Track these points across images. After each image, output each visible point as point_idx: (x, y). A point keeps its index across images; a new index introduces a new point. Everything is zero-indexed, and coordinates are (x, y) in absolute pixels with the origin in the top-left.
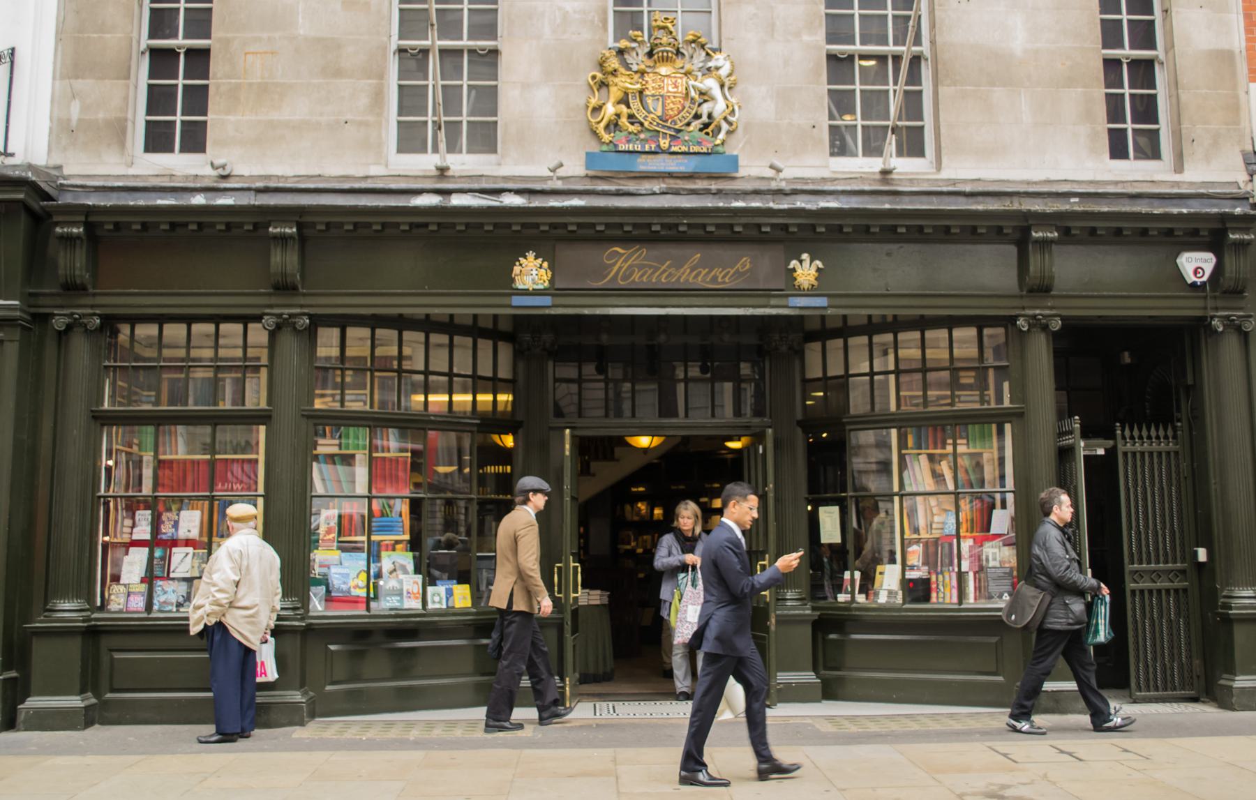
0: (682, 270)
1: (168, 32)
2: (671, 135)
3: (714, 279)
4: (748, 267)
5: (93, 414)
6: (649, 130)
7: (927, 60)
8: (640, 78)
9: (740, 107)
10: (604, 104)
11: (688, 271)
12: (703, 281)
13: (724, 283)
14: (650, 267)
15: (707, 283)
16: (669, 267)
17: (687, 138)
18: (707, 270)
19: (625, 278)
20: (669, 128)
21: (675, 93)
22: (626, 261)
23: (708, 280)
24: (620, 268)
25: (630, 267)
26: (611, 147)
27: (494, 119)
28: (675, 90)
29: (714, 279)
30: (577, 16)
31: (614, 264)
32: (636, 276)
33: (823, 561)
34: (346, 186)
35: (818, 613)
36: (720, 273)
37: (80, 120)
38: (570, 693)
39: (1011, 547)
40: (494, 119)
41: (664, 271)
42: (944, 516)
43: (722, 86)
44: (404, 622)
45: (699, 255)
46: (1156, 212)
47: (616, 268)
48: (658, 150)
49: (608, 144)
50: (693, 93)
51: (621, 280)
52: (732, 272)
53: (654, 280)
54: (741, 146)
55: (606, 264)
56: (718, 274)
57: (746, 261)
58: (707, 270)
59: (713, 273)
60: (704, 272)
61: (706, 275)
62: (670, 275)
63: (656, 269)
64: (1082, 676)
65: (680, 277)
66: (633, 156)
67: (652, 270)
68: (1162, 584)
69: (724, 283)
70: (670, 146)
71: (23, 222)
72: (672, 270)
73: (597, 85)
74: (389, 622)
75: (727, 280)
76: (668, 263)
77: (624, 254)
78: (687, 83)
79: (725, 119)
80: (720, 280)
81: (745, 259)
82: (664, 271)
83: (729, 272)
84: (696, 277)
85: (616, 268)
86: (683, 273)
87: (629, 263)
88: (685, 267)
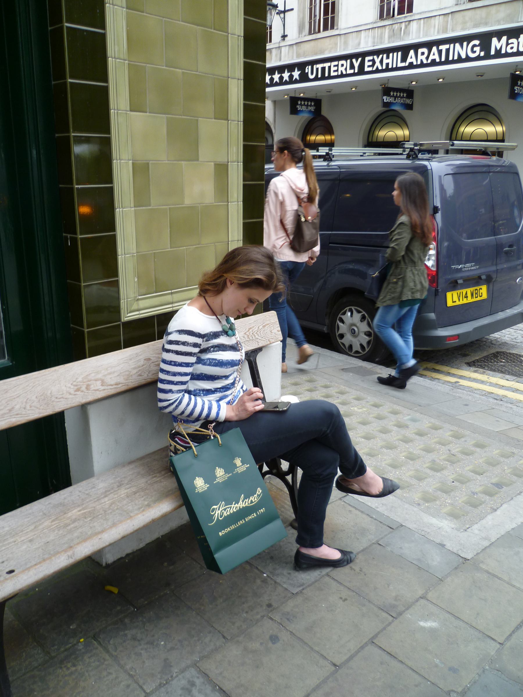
0: (239, 504)
4: (260, 491)
5: (441, 31)
11: (242, 502)
14: (228, 508)
18: (248, 499)
22: (219, 509)
27: (114, 233)
31: (215, 513)
32: (225, 514)
34: (463, 146)
39: (132, 466)
40: (114, 233)
47: (216, 515)
49: (458, 443)
51: (212, 512)
53: (232, 512)
55: (212, 514)
58: (248, 499)
60: (247, 501)
63: (231, 507)
67: (229, 508)
71: (318, 354)
72: (236, 505)
75: (256, 499)
76: (234, 503)
80: (253, 501)
81: (258, 489)
83: (255, 497)
84: (245, 504)
85: (216, 515)
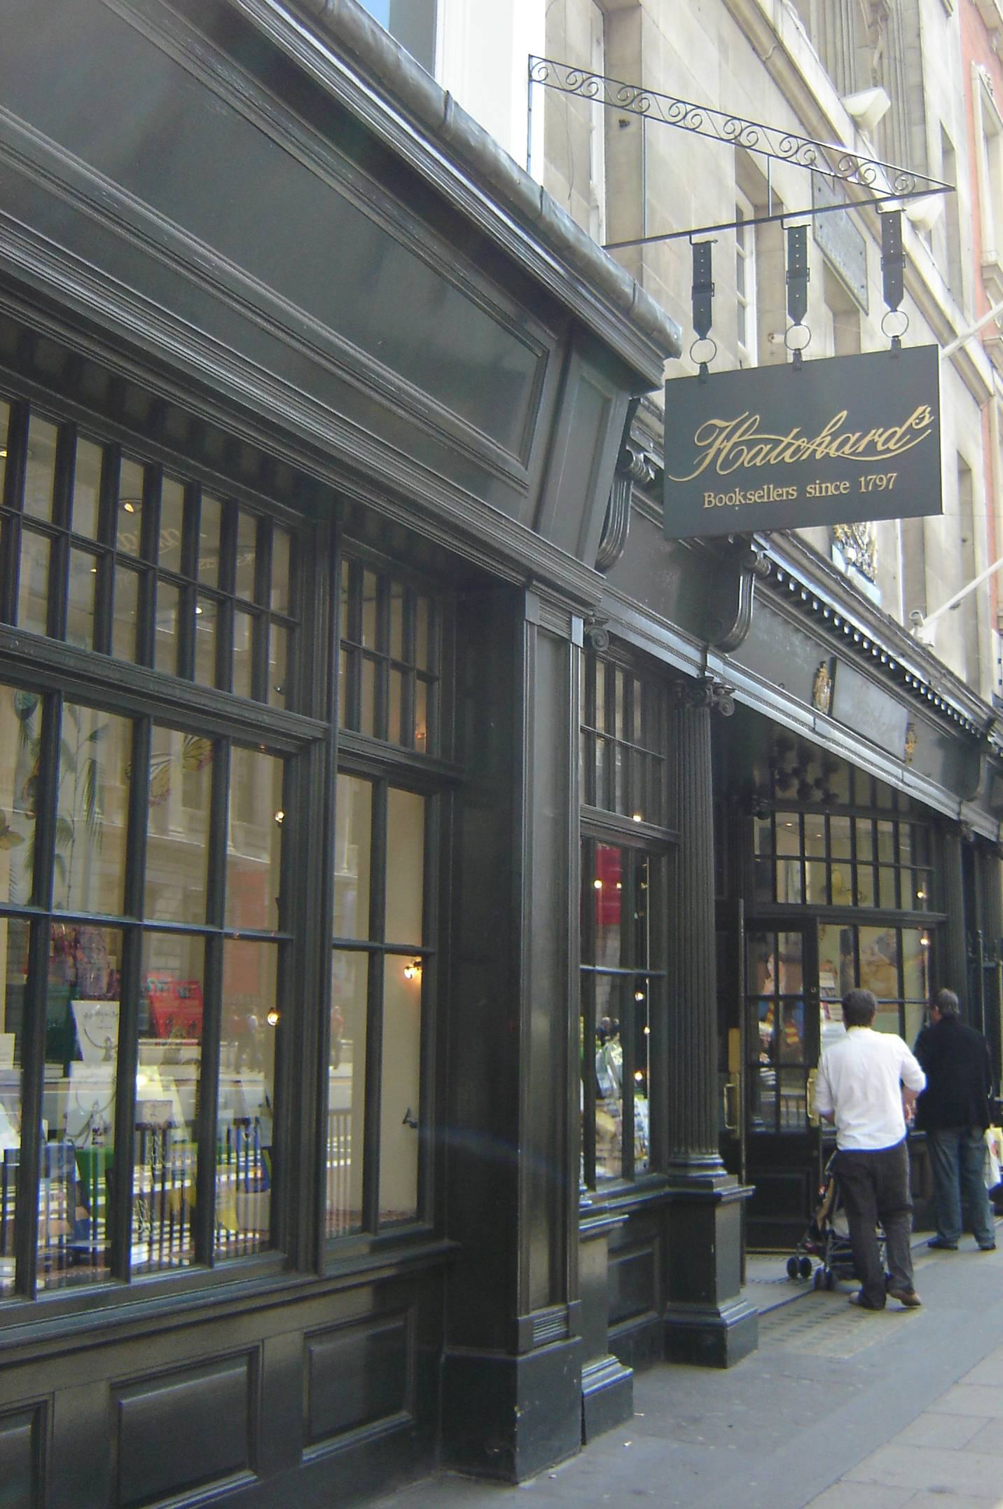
0: (818, 440)
3: (871, 446)
7: (121, 1387)
13: (888, 450)
14: (766, 441)
16: (796, 437)
18: (858, 435)
19: (727, 463)
22: (728, 438)
24: (719, 451)
25: (736, 445)
29: (871, 446)
31: (710, 446)
35: (395, 1256)
36: (880, 436)
37: (106, 1266)
38: (747, 1176)
41: (789, 445)
42: (887, 961)
44: (453, 424)
45: (845, 413)
47: (712, 452)
51: (721, 469)
52: (900, 431)
56: (876, 438)
57: (924, 411)
58: (858, 435)
61: (858, 440)
64: (942, 1157)
65: (815, 451)
68: (706, 1156)
69: (888, 450)
72: (802, 442)
74: (400, 115)
75: (891, 445)
77: (727, 427)
80: (880, 447)
81: (921, 409)
85: (712, 452)
87: (735, 439)
88: (824, 434)
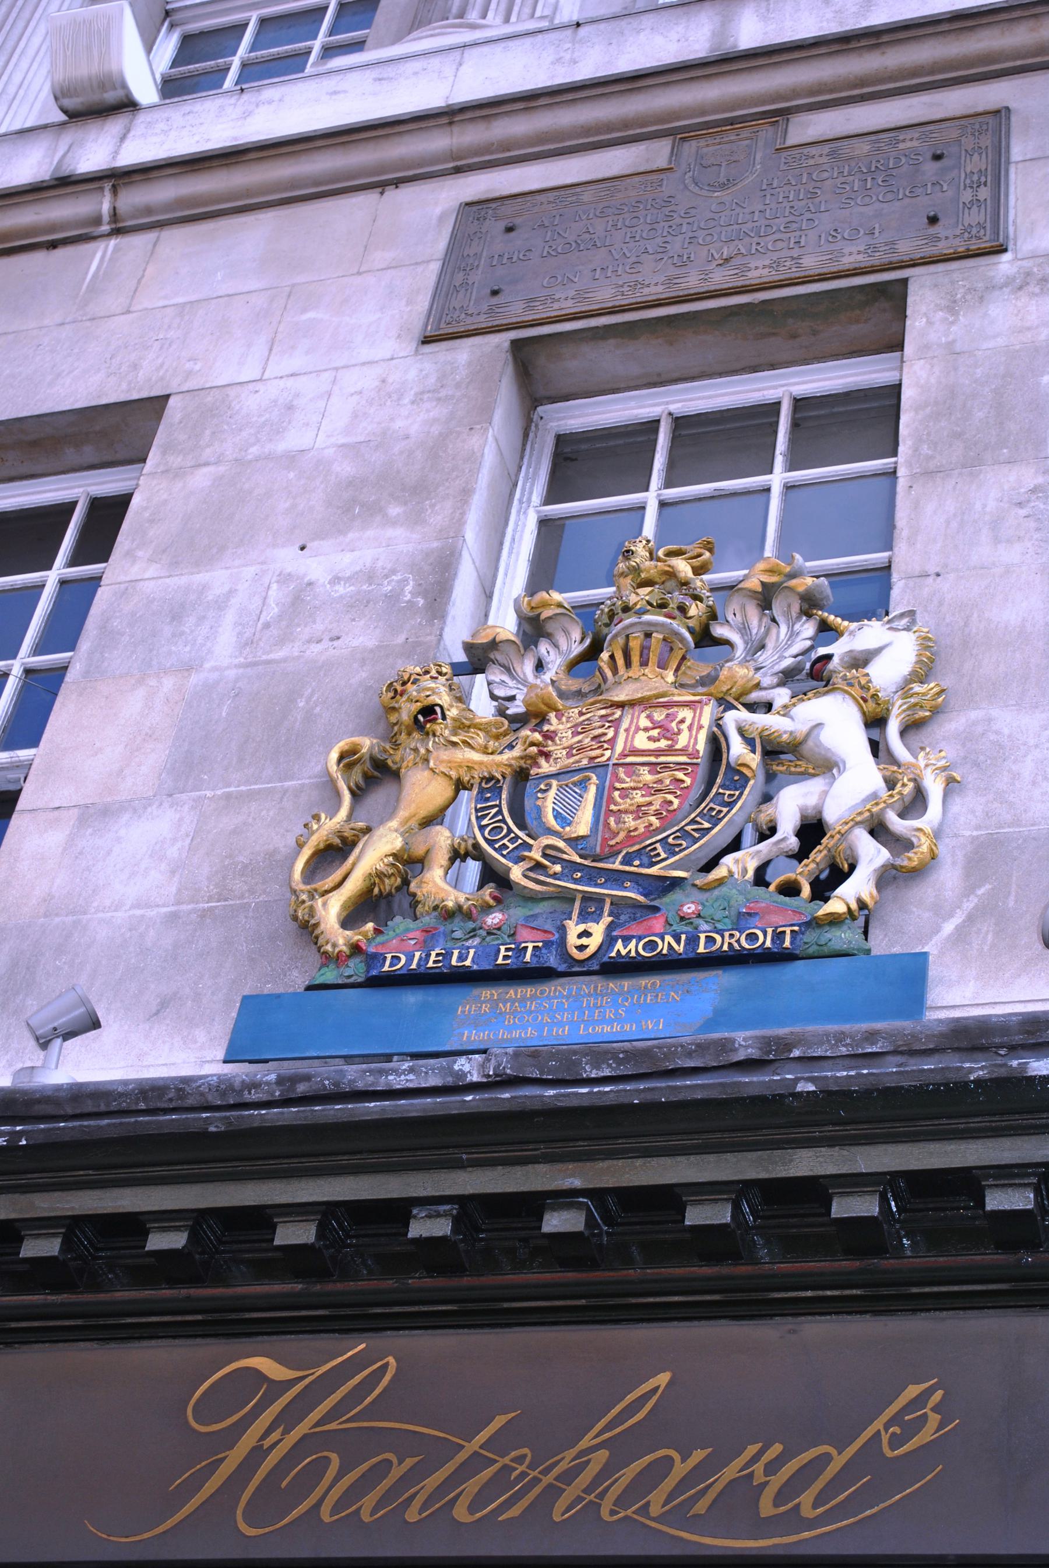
0: (567, 1460)
1: (1037, 1241)
2: (618, 904)
4: (926, 1435)
6: (532, 898)
8: (453, 665)
9: (951, 785)
10: (368, 830)
12: (678, 1515)
13: (794, 1520)
14: (404, 1443)
15: (694, 1523)
16: (497, 1444)
17: (689, 909)
20: (616, 878)
21: (658, 752)
22: (287, 1419)
23: (701, 1507)
24: (258, 1454)
26: (356, 969)
28: (663, 744)
30: (341, 589)
33: (1037, 1219)
36: (772, 1468)
41: (477, 1462)
43: (875, 722)
46: (66, 1295)
48: (552, 960)
50: (737, 748)
54: (949, 928)
59: (731, 1471)
62: (501, 1481)
65: (553, 1493)
66: (447, 995)
70: (609, 940)
73: (357, 775)
78: (718, 722)
79: (878, 830)
80: (766, 1508)
81: (913, 1391)
82: (477, 1462)
83: (826, 1458)
86: (569, 1476)
